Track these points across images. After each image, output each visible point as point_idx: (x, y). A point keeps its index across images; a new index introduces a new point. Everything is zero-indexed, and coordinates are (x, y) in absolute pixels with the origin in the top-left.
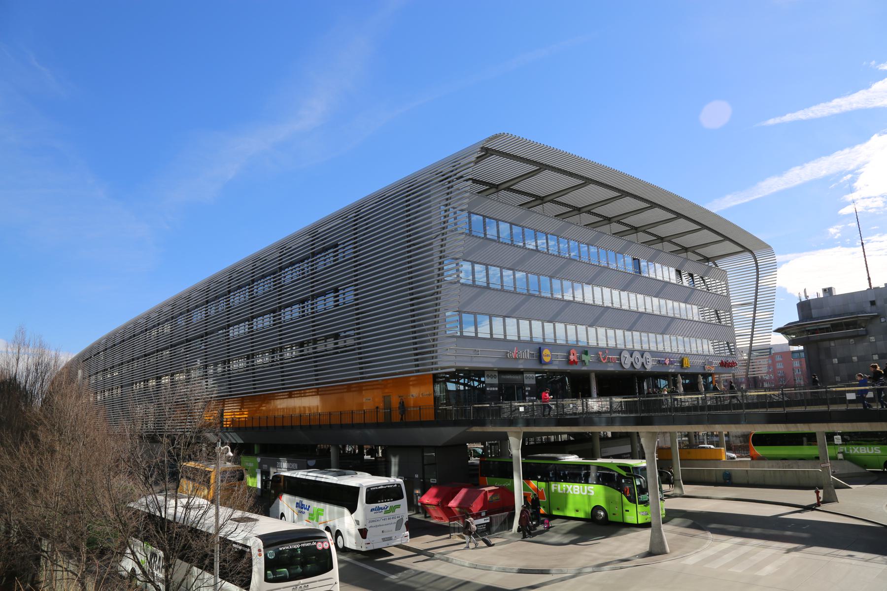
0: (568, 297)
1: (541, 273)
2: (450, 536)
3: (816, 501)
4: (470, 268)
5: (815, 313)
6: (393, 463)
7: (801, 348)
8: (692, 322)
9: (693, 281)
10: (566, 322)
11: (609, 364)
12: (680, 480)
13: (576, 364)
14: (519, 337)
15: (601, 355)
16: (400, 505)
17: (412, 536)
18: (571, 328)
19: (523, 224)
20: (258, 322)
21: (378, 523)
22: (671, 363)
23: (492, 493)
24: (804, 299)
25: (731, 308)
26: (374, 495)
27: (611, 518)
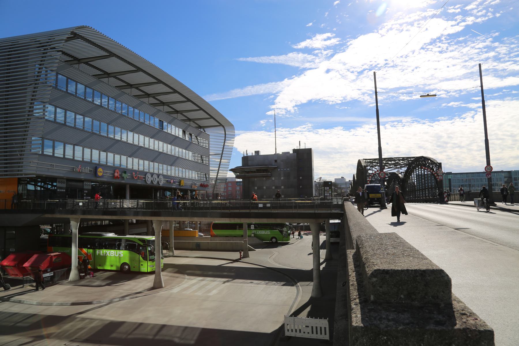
2: (23, 286)
3: (239, 257)
5: (250, 163)
9: (191, 138)
10: (159, 163)
11: (139, 180)
19: (94, 88)
22: (174, 182)
23: (56, 257)
24: (245, 155)
27: (132, 269)
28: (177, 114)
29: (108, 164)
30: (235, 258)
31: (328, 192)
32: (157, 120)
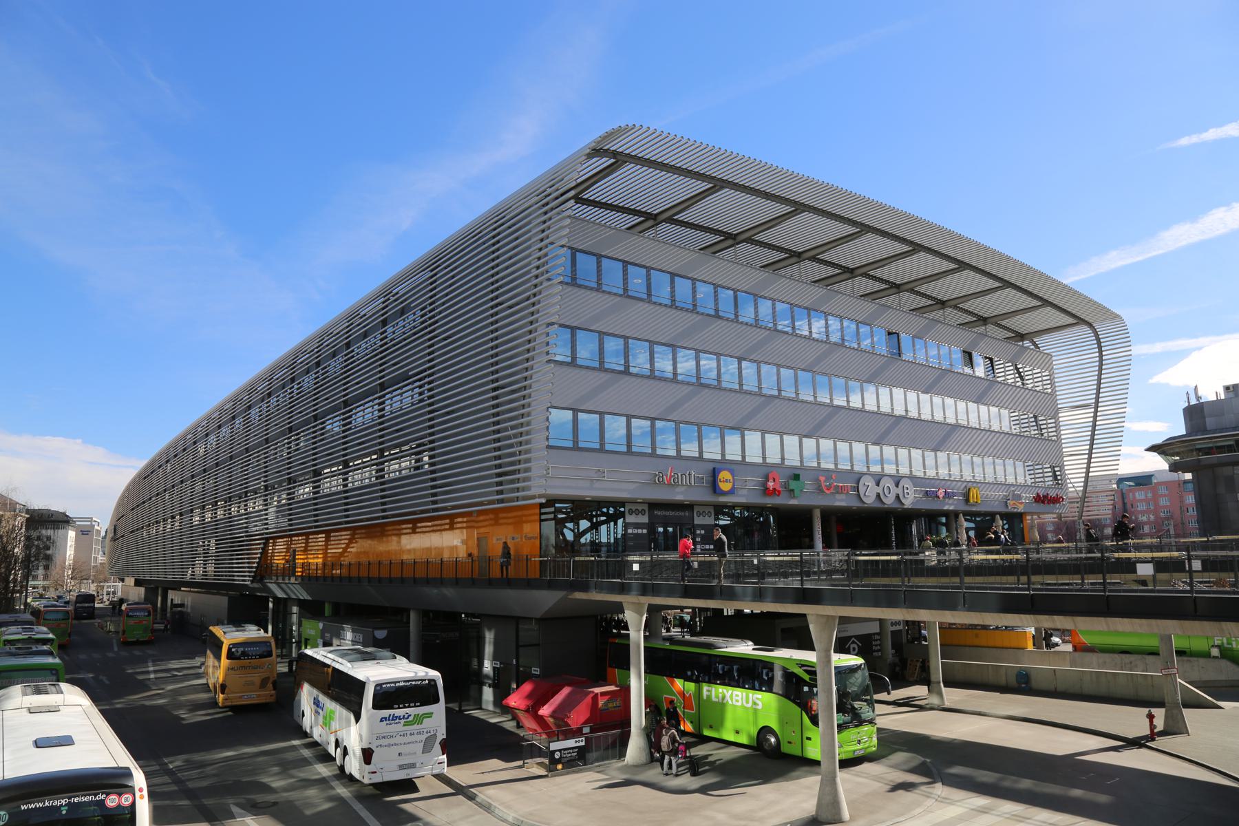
0: (840, 401)
1: (831, 373)
2: (524, 763)
3: (1148, 732)
4: (714, 364)
5: (1210, 422)
6: (487, 640)
7: (1188, 476)
8: (989, 433)
9: (993, 369)
10: (897, 445)
11: (838, 496)
12: (940, 682)
13: (779, 495)
14: (764, 458)
15: (822, 481)
16: (432, 713)
17: (451, 763)
18: (772, 440)
19: (694, 275)
20: (366, 417)
21: (391, 741)
22: (948, 495)
23: (608, 697)
24: (1193, 402)
25: (1057, 413)
26: (389, 697)
27: (786, 749)
29: (786, 463)
30: (1132, 734)
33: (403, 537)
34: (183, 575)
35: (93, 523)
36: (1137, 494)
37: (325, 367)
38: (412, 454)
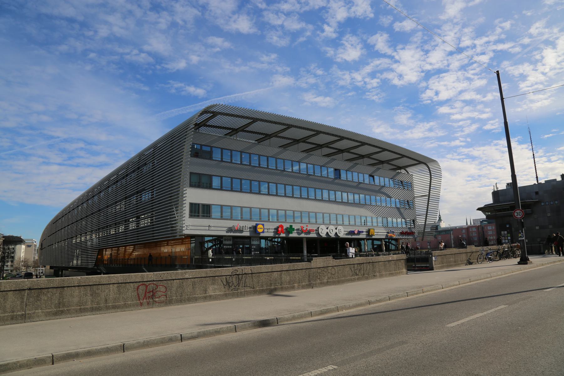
20: (146, 198)
28: (363, 158)
31: (506, 238)
32: (331, 170)
33: (162, 247)
34: (69, 264)
35: (33, 242)
36: (488, 227)
37: (142, 170)
38: (114, 228)
